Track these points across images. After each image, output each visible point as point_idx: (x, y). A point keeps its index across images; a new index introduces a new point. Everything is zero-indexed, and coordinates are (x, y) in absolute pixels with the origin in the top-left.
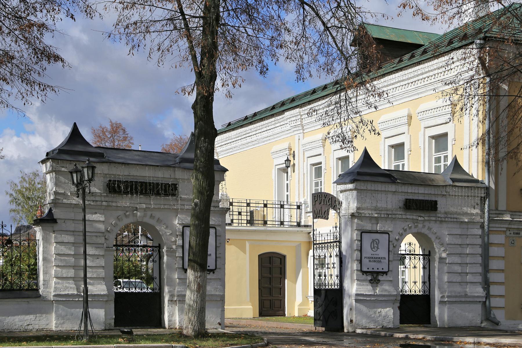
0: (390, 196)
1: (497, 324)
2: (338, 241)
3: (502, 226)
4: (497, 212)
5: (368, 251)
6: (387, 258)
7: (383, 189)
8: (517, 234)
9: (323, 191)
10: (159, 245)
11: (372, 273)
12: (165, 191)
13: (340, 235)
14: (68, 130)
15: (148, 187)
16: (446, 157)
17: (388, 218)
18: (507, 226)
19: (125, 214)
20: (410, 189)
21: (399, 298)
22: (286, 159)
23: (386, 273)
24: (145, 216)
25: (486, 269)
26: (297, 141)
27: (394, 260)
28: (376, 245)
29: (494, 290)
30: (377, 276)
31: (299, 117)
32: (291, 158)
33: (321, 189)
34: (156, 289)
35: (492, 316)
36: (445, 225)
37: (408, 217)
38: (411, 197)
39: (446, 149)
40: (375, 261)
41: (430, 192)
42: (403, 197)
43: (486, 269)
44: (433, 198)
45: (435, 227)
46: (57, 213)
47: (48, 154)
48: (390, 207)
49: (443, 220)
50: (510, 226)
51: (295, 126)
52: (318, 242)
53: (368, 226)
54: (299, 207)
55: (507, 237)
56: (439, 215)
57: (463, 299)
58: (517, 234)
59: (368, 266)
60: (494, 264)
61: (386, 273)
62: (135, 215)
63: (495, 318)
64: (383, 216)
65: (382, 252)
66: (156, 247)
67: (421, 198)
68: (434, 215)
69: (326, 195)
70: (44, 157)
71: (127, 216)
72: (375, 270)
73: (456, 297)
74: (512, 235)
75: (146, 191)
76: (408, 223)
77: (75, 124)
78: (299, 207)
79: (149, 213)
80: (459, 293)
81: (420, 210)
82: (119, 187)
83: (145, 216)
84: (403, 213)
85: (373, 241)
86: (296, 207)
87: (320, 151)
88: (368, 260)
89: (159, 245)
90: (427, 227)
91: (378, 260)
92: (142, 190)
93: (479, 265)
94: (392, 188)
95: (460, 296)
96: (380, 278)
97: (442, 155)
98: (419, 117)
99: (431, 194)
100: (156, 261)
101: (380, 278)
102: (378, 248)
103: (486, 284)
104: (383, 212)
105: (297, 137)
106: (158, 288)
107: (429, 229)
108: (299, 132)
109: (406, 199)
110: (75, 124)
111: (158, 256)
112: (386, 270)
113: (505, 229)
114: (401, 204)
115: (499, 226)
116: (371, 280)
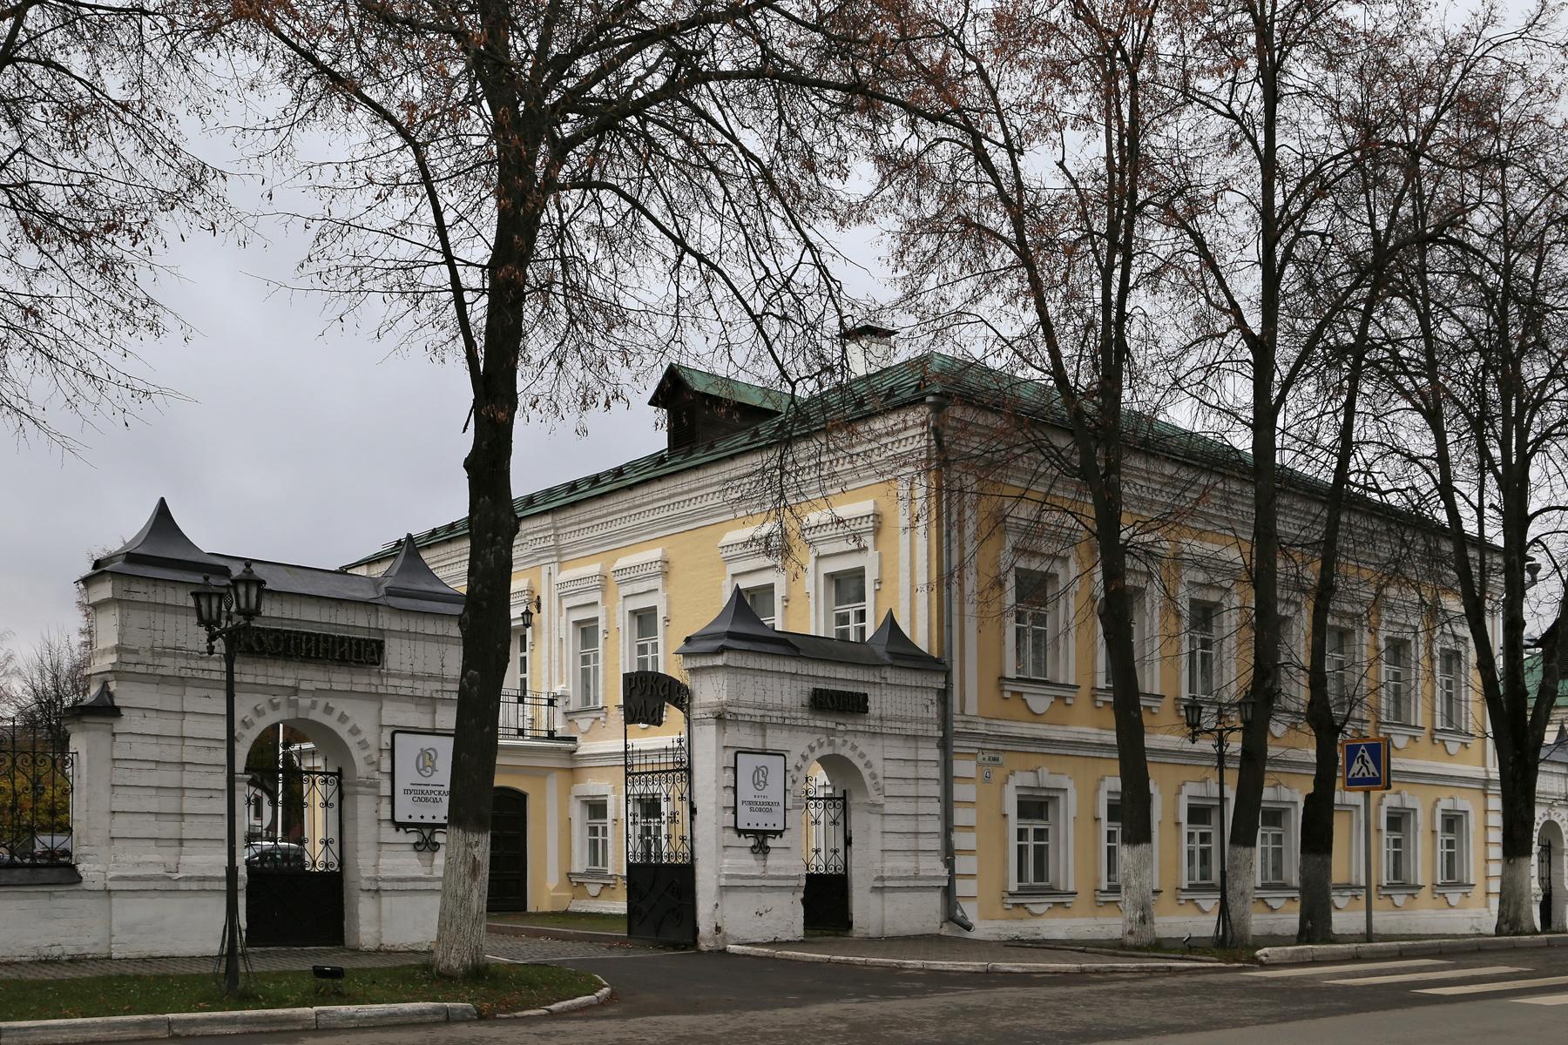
0: (787, 682)
1: (968, 928)
2: (685, 770)
3: (972, 744)
4: (965, 718)
5: (747, 791)
6: (782, 804)
7: (776, 668)
8: (994, 759)
9: (661, 671)
10: (340, 770)
11: (755, 833)
12: (358, 654)
13: (689, 757)
14: (142, 517)
15: (322, 645)
16: (861, 615)
17: (783, 724)
18: (979, 745)
19: (271, 701)
20: (821, 670)
21: (803, 882)
22: (524, 610)
23: (779, 833)
24: (314, 706)
25: (949, 829)
26: (545, 577)
27: (794, 807)
28: (762, 779)
29: (963, 864)
30: (765, 838)
31: (552, 532)
32: (533, 610)
33: (655, 660)
34: (333, 865)
35: (959, 913)
36: (879, 742)
37: (819, 723)
38: (821, 686)
39: (861, 597)
40: (760, 810)
41: (855, 677)
42: (809, 686)
43: (949, 829)
44: (861, 690)
45: (862, 744)
46: (123, 694)
47: (97, 564)
48: (786, 702)
49: (878, 731)
50: (983, 746)
51: (543, 550)
52: (636, 770)
53: (748, 738)
54: (551, 703)
55: (978, 764)
56: (872, 723)
57: (912, 884)
58: (994, 759)
59: (747, 819)
60: (961, 816)
61: (779, 833)
62: (294, 704)
63: (964, 917)
64: (774, 720)
65: (774, 792)
66: (332, 774)
67: (839, 688)
68: (862, 722)
69: (657, 677)
70: (87, 569)
71: (275, 707)
72: (762, 827)
73: (900, 878)
74: (987, 761)
75: (317, 652)
76: (818, 736)
77: (162, 500)
78: (551, 703)
79: (322, 702)
80: (906, 871)
81: (839, 711)
82: (261, 643)
83: (314, 706)
84: (806, 715)
85: (758, 769)
86: (546, 702)
87: (596, 596)
88: (748, 807)
89: (340, 770)
90: (849, 744)
91: (766, 807)
92: (309, 651)
93: (935, 818)
94: (791, 666)
95: (907, 878)
96: (770, 842)
97: (851, 610)
98: (724, 555)
99: (857, 681)
100: (332, 805)
101: (770, 842)
102: (765, 784)
103: (949, 854)
104: (775, 714)
105: (545, 570)
106: (336, 863)
107: (854, 748)
108: (550, 560)
109: (815, 689)
110: (162, 500)
111: (337, 792)
112: (780, 827)
113: (976, 751)
114: (805, 699)
115: (1430, 763)
116: (754, 847)
